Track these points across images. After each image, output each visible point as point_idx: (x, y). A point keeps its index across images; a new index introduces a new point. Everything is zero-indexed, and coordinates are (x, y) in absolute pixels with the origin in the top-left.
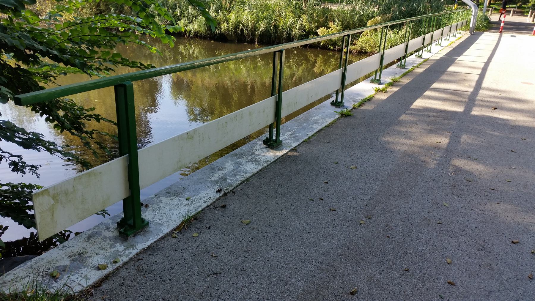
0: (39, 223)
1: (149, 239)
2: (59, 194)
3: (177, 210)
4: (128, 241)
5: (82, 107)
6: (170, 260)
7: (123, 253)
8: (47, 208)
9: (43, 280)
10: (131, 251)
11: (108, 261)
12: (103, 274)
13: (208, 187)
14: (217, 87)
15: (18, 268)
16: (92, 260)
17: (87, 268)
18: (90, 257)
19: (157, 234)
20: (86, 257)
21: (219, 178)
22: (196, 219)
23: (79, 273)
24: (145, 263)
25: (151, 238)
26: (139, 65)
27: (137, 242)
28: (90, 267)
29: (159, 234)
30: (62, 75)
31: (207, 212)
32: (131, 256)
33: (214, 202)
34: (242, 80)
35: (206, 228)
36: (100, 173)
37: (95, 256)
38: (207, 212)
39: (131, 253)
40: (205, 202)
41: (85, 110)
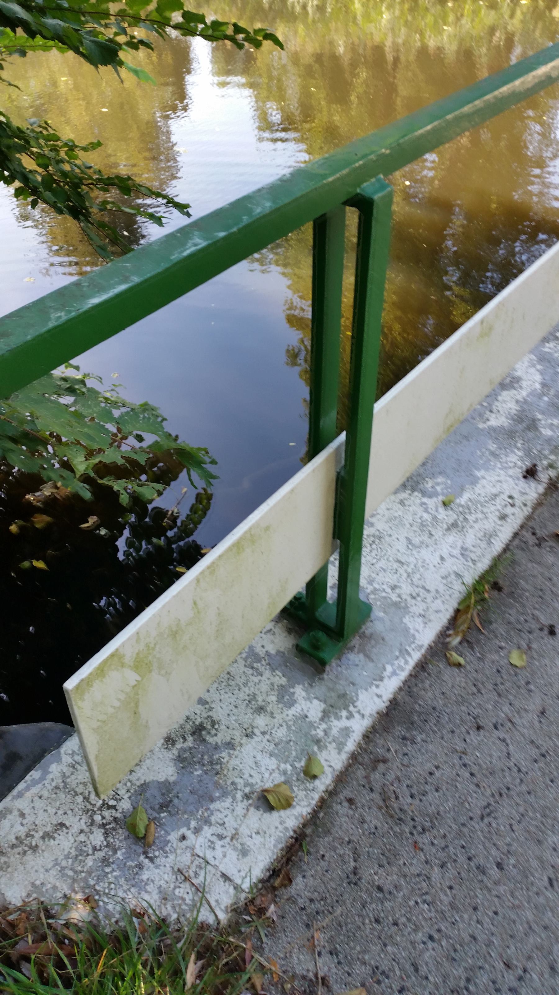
0: (97, 756)
1: (385, 669)
2: (152, 645)
3: (431, 549)
4: (325, 676)
5: (73, 141)
6: (475, 769)
7: (326, 732)
8: (117, 704)
9: (108, 846)
10: (344, 723)
11: (289, 768)
12: (286, 829)
13: (493, 454)
14: (319, 58)
15: (28, 788)
16: (237, 762)
17: (230, 800)
18: (230, 745)
19: (404, 652)
20: (216, 747)
21: (513, 420)
22: (496, 587)
23: (213, 819)
24: (398, 779)
25: (389, 668)
26: (230, 31)
27: (353, 684)
28: (239, 795)
29: (407, 650)
30: (16, 57)
31: (520, 555)
32: (351, 746)
33: (529, 518)
34: (377, 39)
35: (541, 629)
36: (267, 528)
37: (244, 740)
38: (520, 555)
39: (346, 732)
40: (503, 517)
41: (78, 149)
